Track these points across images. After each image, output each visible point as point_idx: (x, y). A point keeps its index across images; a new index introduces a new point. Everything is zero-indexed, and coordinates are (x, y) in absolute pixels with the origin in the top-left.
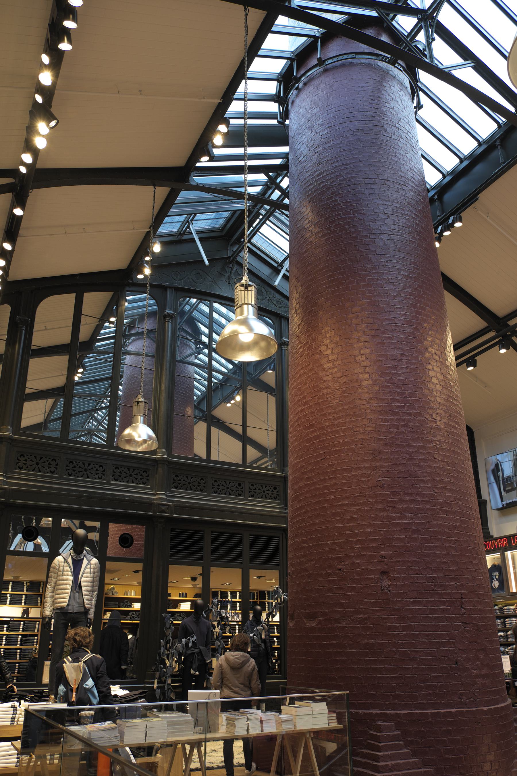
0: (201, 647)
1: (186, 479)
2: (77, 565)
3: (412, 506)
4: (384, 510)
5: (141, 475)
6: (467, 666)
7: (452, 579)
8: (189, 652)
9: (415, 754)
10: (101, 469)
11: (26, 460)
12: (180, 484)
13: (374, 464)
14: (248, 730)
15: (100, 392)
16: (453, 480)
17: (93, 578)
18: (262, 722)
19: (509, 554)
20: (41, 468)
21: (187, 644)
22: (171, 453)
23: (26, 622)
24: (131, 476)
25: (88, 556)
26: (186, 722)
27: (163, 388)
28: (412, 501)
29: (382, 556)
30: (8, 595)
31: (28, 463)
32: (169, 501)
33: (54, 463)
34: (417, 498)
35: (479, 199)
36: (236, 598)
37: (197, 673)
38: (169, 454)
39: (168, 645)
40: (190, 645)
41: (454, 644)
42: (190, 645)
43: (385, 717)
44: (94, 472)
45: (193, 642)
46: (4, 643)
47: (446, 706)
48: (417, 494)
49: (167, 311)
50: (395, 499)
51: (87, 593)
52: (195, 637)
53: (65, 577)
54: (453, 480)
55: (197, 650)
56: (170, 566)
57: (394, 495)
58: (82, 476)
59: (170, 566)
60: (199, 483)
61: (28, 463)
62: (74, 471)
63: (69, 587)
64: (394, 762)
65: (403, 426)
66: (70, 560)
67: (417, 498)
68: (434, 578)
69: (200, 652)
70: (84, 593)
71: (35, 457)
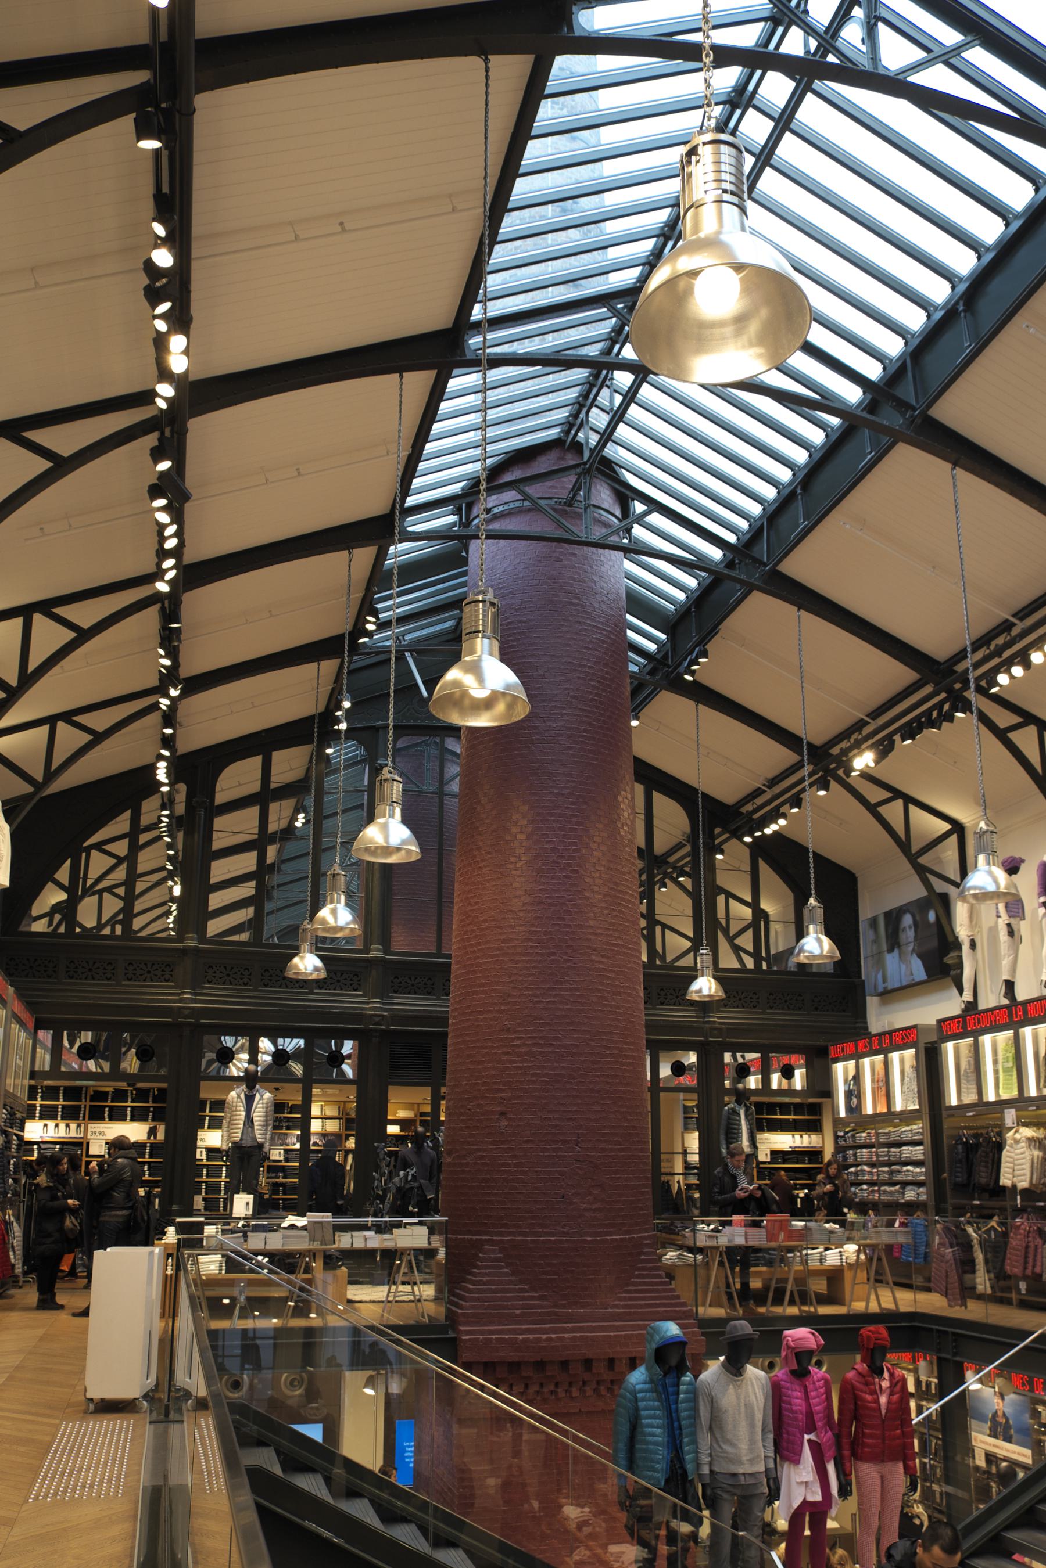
0: (422, 1181)
1: (409, 981)
2: (250, 1100)
3: (534, 1049)
4: (508, 1053)
5: (351, 980)
7: (569, 1120)
8: (408, 1186)
9: (513, 1274)
11: (215, 972)
12: (400, 987)
13: (503, 1008)
14: (352, 1244)
15: (940, 69)
16: (585, 1021)
17: (266, 1112)
18: (366, 1239)
19: (1027, 1032)
20: (232, 980)
21: (406, 1176)
22: (389, 948)
23: (152, 1165)
24: (338, 981)
25: (261, 1090)
26: (303, 1237)
28: (534, 1045)
29: (502, 1098)
32: (385, 1010)
33: (246, 973)
34: (541, 1041)
35: (720, 631)
37: (416, 1210)
38: (386, 950)
39: (383, 1179)
40: (409, 1178)
41: (563, 1179)
42: (409, 1178)
43: (491, 1242)
45: (413, 1175)
46: (224, 1175)
48: (541, 1038)
49: (379, 762)
50: (518, 1042)
51: (260, 1127)
52: (415, 1170)
53: (238, 1113)
54: (585, 1021)
55: (416, 1184)
56: (390, 1087)
57: (519, 1038)
58: (280, 987)
59: (390, 1087)
60: (425, 984)
62: (271, 980)
63: (242, 1122)
64: (488, 1278)
65: (534, 967)
66: (243, 1096)
67: (541, 1041)
68: (549, 1119)
69: (420, 1187)
70: (256, 1127)
71: (225, 968)
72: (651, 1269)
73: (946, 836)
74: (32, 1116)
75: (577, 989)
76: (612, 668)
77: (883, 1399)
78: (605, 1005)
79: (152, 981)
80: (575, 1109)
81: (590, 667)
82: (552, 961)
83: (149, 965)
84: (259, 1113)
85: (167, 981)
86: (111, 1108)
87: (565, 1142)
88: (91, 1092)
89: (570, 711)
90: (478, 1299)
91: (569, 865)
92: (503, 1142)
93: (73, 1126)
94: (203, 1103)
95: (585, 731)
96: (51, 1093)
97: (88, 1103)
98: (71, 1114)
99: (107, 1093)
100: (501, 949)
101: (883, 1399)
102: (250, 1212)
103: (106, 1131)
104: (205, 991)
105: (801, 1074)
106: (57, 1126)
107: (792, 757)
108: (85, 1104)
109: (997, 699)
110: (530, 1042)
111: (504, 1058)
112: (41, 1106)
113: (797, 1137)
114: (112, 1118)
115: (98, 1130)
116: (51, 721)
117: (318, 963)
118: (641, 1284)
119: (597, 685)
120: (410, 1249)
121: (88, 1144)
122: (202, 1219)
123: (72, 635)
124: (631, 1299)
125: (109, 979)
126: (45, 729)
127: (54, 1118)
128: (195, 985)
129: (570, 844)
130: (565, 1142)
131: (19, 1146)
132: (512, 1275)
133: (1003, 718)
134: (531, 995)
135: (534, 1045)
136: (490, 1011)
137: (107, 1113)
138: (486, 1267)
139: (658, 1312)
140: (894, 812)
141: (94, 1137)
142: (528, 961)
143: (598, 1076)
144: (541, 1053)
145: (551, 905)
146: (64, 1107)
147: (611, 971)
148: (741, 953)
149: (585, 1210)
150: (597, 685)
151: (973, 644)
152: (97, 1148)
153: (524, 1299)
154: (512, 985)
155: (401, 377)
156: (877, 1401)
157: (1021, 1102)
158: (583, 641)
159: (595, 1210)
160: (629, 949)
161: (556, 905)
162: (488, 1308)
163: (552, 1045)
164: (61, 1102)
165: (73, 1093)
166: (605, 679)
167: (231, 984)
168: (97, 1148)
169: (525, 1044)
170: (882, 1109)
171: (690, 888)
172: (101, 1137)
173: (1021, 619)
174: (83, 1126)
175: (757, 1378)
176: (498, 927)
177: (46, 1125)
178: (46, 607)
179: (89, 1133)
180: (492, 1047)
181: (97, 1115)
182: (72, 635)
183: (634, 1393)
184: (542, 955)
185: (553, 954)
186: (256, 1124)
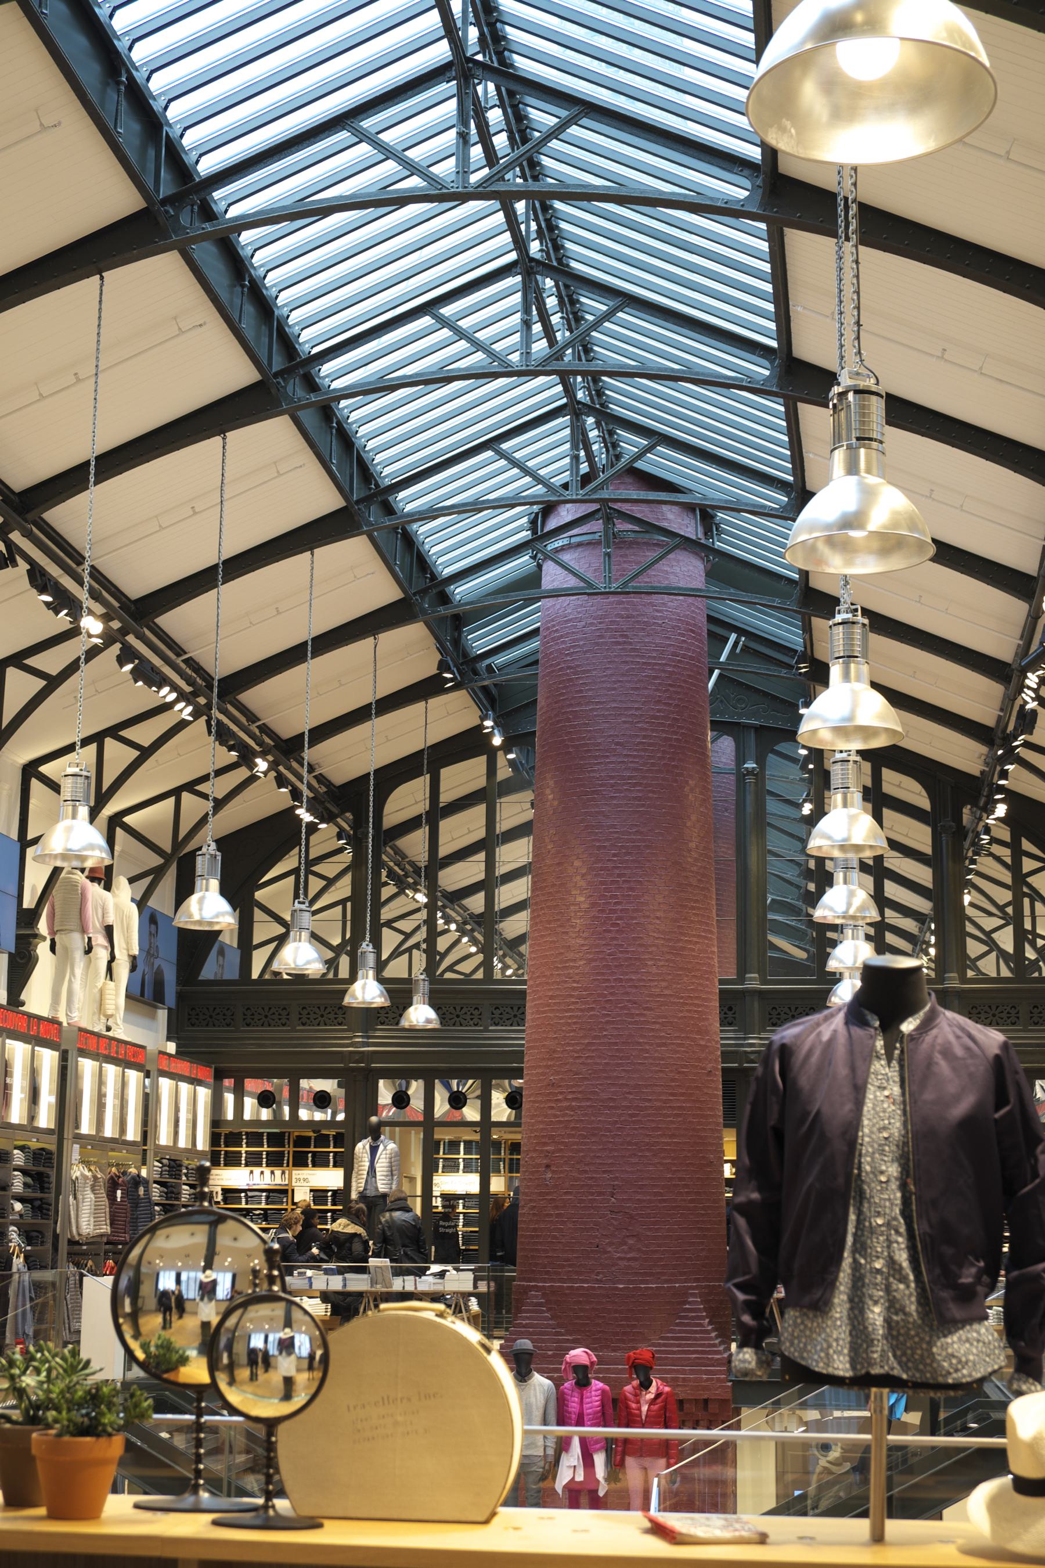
2: (374, 1150)
4: (552, 1108)
6: (609, 1249)
7: (604, 1172)
10: (476, 1012)
24: (515, 1016)
28: (574, 1099)
29: (548, 1151)
30: (461, 1160)
34: (579, 1096)
36: (240, 1203)
38: (964, 979)
44: (468, 1017)
46: (461, 1224)
47: (584, 1281)
57: (561, 1093)
58: (454, 1025)
63: (365, 1173)
65: (575, 1023)
66: (368, 1147)
67: (579, 1096)
68: (585, 1172)
70: (378, 1178)
72: (693, 1318)
75: (616, 1044)
77: (645, 1408)
78: (645, 1058)
79: (326, 1025)
80: (610, 1161)
81: (637, 709)
82: (591, 1017)
83: (322, 1008)
85: (340, 1024)
86: (314, 1154)
87: (600, 1194)
89: (613, 759)
91: (610, 919)
92: (548, 1194)
93: (278, 1172)
94: (438, 1143)
95: (630, 778)
97: (292, 1149)
98: (275, 1161)
101: (645, 1408)
103: (310, 1178)
106: (262, 1173)
108: (289, 1150)
112: (246, 1152)
114: (227, 1164)
115: (302, 1177)
116: (176, 793)
117: (432, 1014)
118: (680, 1332)
121: (293, 1190)
124: (665, 1345)
125: (284, 1025)
126: (171, 801)
127: (260, 1165)
129: (611, 897)
132: (551, 1319)
134: (572, 1051)
135: (574, 1099)
137: (310, 1159)
139: (689, 1359)
141: (298, 1184)
142: (570, 1017)
143: (635, 1129)
144: (579, 1107)
146: (268, 1153)
147: (654, 1023)
149: (620, 1258)
152: (302, 1196)
153: (558, 1341)
154: (556, 1041)
155: (312, 554)
156: (639, 1409)
158: (629, 682)
159: (629, 1259)
160: (682, 998)
161: (596, 960)
163: (589, 1099)
164: (265, 1148)
168: (302, 1196)
169: (566, 1099)
171: (1008, 860)
172: (305, 1184)
174: (287, 1172)
175: (541, 1385)
176: (547, 983)
177: (252, 1172)
178: (113, 731)
179: (294, 1180)
181: (300, 1162)
182: (137, 753)
184: (582, 1010)
185: (592, 1009)
186: (378, 1174)
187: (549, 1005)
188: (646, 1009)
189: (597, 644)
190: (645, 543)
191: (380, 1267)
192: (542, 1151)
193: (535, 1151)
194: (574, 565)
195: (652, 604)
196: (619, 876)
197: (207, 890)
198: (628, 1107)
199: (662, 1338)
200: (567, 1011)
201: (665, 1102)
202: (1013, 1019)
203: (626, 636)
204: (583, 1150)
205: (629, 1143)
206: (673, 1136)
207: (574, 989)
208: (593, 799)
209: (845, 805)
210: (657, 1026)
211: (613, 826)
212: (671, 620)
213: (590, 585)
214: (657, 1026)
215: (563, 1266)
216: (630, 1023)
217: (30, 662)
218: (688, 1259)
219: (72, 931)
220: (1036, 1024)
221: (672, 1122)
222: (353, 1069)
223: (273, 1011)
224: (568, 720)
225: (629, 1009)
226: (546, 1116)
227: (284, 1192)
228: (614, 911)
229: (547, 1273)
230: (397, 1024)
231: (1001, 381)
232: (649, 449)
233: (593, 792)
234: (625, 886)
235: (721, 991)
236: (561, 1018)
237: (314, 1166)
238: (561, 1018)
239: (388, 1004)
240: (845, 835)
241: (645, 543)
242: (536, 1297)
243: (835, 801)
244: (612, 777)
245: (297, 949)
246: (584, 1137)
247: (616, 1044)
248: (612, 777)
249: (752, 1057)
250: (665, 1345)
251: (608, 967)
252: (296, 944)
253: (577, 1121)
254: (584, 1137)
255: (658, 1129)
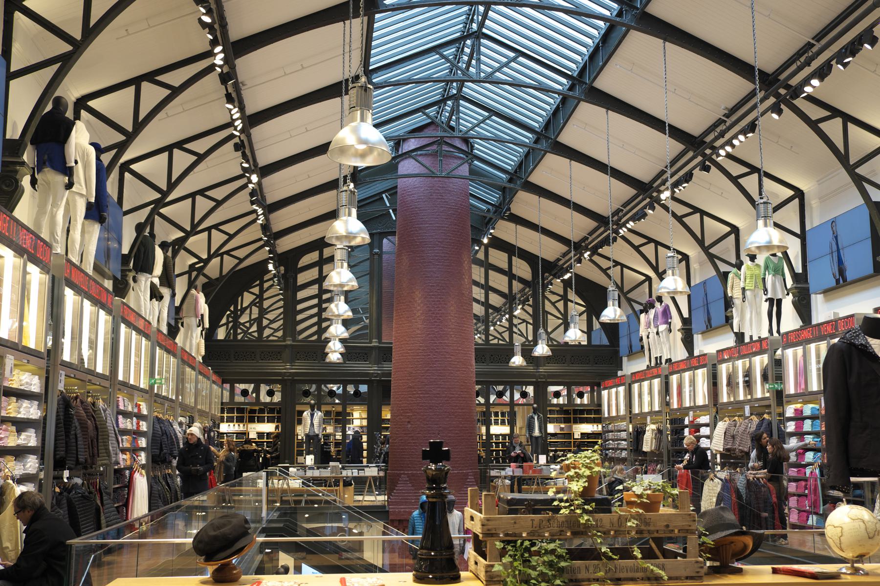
2: (312, 415)
9: (412, 486)
27: (374, 302)
28: (421, 394)
31: (302, 356)
38: (380, 342)
53: (470, 353)
56: (383, 407)
61: (302, 356)
66: (309, 414)
73: (643, 282)
74: (223, 422)
75: (440, 370)
76: (458, 226)
81: (447, 227)
84: (316, 421)
85: (279, 360)
87: (434, 433)
88: (248, 410)
90: (397, 496)
92: (409, 434)
93: (241, 425)
95: (445, 257)
96: (231, 411)
97: (248, 415)
98: (240, 420)
99: (256, 410)
100: (408, 353)
102: (313, 463)
104: (296, 364)
105: (703, 374)
106: (234, 425)
107: (565, 248)
108: (246, 415)
109: (810, 98)
110: (420, 392)
111: (410, 399)
112: (227, 416)
113: (595, 426)
114: (258, 422)
119: (450, 235)
120: (370, 476)
121: (248, 433)
122: (288, 465)
123: (195, 158)
124: (461, 496)
127: (233, 422)
128: (292, 361)
130: (434, 433)
131: (218, 436)
133: (816, 113)
135: (421, 394)
136: (404, 380)
138: (402, 484)
140: (833, 128)
142: (419, 358)
145: (429, 334)
148: (715, 260)
150: (450, 235)
151: (612, 214)
157: (651, 413)
162: (401, 499)
164: (236, 414)
165: (241, 410)
166: (455, 231)
167: (308, 360)
168: (577, 436)
170: (692, 404)
173: (625, 208)
175: (458, 514)
176: (407, 344)
180: (405, 395)
181: (252, 420)
182: (227, 237)
183: (413, 518)
184: (425, 356)
185: (429, 355)
187: (408, 353)
188: (452, 355)
189: (430, 198)
190: (449, 156)
191: (335, 466)
192: (406, 416)
193: (402, 415)
194: (424, 162)
195: (452, 183)
196: (440, 298)
197: (340, 301)
198: (446, 397)
199: (459, 494)
200: (417, 356)
201: (459, 395)
202: (564, 362)
203: (442, 196)
204: (426, 415)
205: (446, 412)
206: (462, 409)
207: (420, 346)
208: (428, 265)
209: (673, 275)
210: (456, 363)
211: (437, 277)
212: (460, 190)
213: (433, 173)
214: (456, 363)
215: (416, 464)
216: (445, 361)
217: (208, 193)
218: (468, 460)
219: (191, 317)
220: (572, 364)
221: (462, 403)
222: (286, 380)
223: (248, 354)
224: (417, 231)
225: (445, 355)
226: (408, 401)
227: (245, 434)
228: (439, 313)
229: (409, 467)
230: (324, 360)
231: (698, 105)
232: (488, 118)
233: (428, 262)
234: (443, 303)
235: (475, 349)
236: (415, 359)
237: (258, 422)
238: (415, 359)
239: (345, 352)
240: (675, 287)
241: (449, 156)
242: (404, 477)
243: (669, 273)
244: (437, 256)
245: (336, 327)
246: (426, 409)
247: (440, 370)
248: (437, 256)
249: (542, 377)
250: (461, 496)
251: (436, 337)
252: (335, 325)
253: (423, 403)
254: (426, 409)
255: (456, 406)
